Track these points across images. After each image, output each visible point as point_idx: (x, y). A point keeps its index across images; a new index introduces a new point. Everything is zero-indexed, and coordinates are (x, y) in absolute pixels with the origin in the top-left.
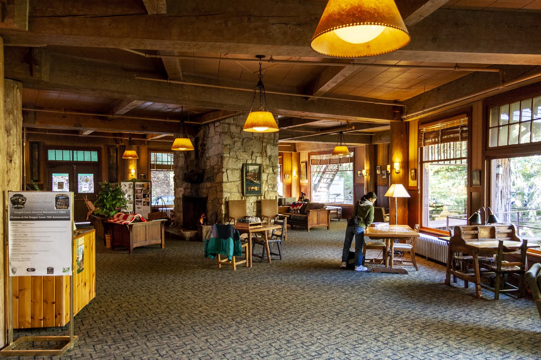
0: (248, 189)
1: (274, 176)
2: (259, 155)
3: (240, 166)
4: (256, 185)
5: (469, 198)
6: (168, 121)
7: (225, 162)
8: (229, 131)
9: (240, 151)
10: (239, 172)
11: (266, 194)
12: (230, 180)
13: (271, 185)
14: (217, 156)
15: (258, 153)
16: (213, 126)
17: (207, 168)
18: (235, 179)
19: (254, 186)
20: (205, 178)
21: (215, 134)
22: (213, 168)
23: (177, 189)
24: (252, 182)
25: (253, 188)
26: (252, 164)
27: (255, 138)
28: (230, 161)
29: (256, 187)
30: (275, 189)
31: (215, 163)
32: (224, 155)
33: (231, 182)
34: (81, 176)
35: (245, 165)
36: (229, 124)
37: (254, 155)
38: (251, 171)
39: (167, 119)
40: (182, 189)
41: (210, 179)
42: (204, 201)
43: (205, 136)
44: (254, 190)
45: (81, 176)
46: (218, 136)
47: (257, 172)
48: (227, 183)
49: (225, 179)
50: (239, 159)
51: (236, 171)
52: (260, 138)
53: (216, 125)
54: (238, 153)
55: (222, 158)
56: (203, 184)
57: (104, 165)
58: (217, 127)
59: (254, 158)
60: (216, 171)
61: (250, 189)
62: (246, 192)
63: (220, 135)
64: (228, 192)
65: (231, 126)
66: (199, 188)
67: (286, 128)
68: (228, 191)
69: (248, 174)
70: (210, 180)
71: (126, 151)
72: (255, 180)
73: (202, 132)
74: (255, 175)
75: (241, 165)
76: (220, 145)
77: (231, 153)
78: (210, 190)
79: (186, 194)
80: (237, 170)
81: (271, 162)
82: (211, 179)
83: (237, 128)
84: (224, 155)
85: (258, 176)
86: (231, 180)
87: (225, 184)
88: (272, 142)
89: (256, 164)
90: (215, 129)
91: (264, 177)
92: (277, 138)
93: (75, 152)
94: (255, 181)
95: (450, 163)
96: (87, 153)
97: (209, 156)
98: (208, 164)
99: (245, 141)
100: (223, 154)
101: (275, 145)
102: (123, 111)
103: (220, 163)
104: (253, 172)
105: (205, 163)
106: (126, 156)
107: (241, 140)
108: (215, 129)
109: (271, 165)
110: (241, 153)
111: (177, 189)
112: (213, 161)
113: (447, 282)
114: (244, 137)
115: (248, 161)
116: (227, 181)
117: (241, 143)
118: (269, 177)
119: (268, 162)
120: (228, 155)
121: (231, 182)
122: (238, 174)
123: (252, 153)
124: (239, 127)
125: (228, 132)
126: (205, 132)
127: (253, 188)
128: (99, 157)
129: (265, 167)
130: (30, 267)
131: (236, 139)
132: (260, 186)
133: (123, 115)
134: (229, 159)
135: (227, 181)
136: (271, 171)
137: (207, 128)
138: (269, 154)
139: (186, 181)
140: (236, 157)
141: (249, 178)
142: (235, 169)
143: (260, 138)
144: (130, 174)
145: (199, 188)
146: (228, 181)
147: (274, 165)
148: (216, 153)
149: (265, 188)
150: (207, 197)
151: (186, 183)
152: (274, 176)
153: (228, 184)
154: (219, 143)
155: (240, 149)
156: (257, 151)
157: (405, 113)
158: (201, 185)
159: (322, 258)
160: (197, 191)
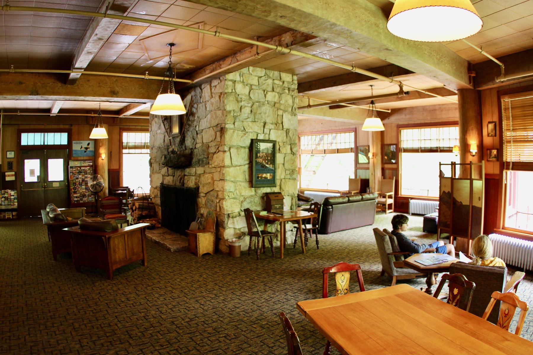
0: (258, 177)
1: (293, 158)
2: (272, 127)
3: (248, 143)
4: (268, 171)
6: (147, 77)
9: (248, 120)
10: (247, 150)
11: (282, 184)
12: (234, 163)
13: (289, 170)
14: (215, 128)
16: (208, 86)
17: (198, 146)
19: (266, 173)
20: (194, 160)
24: (263, 166)
25: (264, 175)
26: (263, 141)
27: (268, 103)
28: (235, 134)
29: (269, 175)
30: (294, 176)
33: (236, 166)
34: (52, 163)
35: (253, 143)
36: (234, 82)
38: (263, 150)
39: (145, 74)
41: (203, 161)
42: (194, 193)
44: (266, 178)
45: (52, 163)
47: (270, 152)
50: (247, 133)
52: (275, 103)
53: (213, 84)
55: (222, 131)
58: (216, 86)
61: (261, 177)
62: (256, 181)
64: (232, 181)
66: (185, 175)
68: (232, 180)
69: (259, 155)
70: (200, 163)
72: (268, 164)
74: (267, 156)
80: (245, 148)
81: (289, 138)
83: (245, 87)
84: (227, 126)
85: (271, 158)
87: (228, 169)
89: (268, 141)
91: (279, 158)
94: (267, 166)
97: (200, 128)
100: (225, 124)
104: (265, 151)
108: (211, 90)
109: (288, 142)
110: (250, 124)
115: (259, 135)
116: (230, 165)
120: (232, 126)
121: (236, 166)
122: (245, 153)
125: (232, 92)
127: (264, 175)
129: (281, 144)
130: (478, 200)
132: (274, 172)
134: (234, 132)
136: (289, 151)
138: (286, 126)
139: (167, 165)
140: (242, 129)
141: (260, 160)
142: (241, 147)
143: (275, 103)
144: (100, 159)
145: (185, 175)
146: (232, 165)
148: (214, 123)
149: (280, 174)
150: (197, 189)
151: (166, 168)
153: (232, 169)
155: (248, 118)
156: (271, 122)
159: (429, 240)
160: (182, 180)
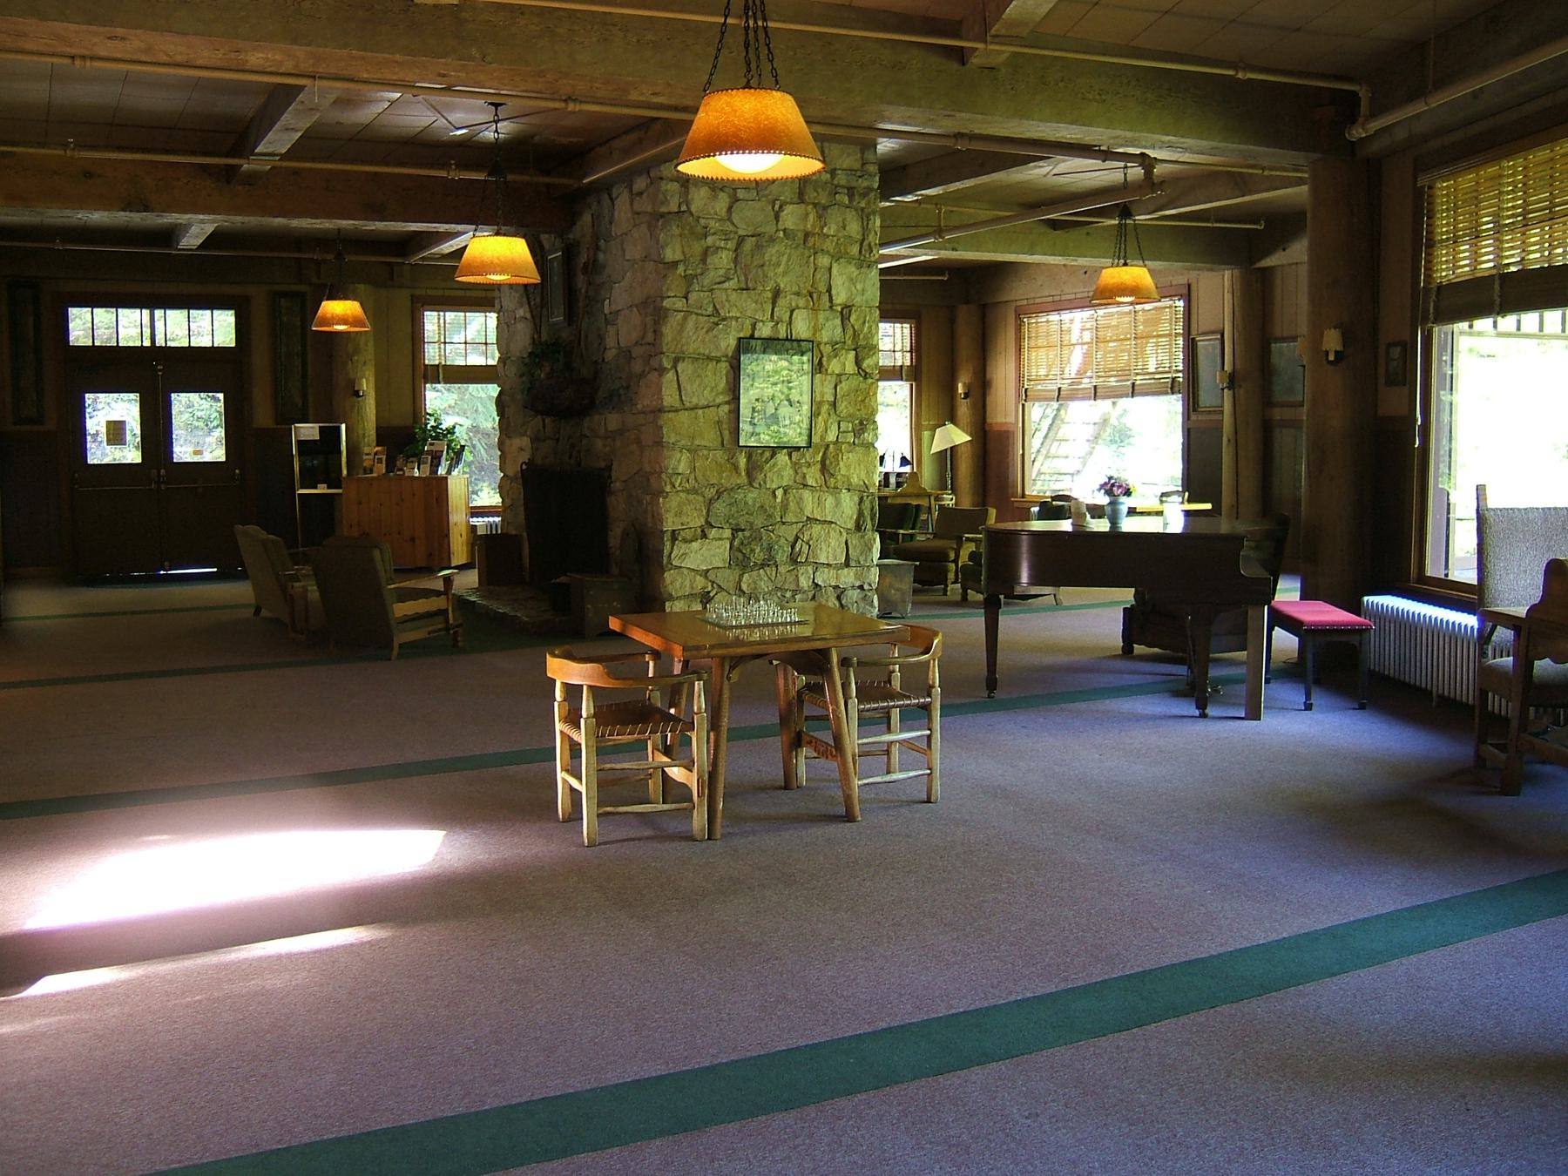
5: (1186, 443)
7: (668, 331)
8: (684, 208)
9: (726, 285)
15: (798, 294)
18: (706, 396)
21: (635, 226)
22: (627, 355)
23: (508, 442)
28: (690, 324)
30: (868, 436)
31: (635, 336)
32: (666, 303)
37: (781, 302)
40: (525, 442)
43: (599, 237)
46: (644, 228)
48: (677, 411)
49: (669, 397)
50: (724, 319)
51: (711, 365)
53: (636, 188)
54: (720, 296)
56: (597, 417)
57: (260, 360)
59: (781, 312)
60: (637, 367)
63: (649, 227)
65: (692, 189)
67: (909, 198)
71: (324, 303)
73: (587, 218)
75: (733, 343)
76: (650, 266)
77: (693, 297)
78: (618, 443)
79: (539, 461)
81: (850, 332)
82: (620, 398)
84: (666, 303)
86: (695, 401)
87: (671, 415)
88: (855, 250)
90: (632, 204)
92: (873, 239)
93: (159, 313)
95: (1471, 327)
96: (202, 317)
97: (614, 308)
98: (610, 342)
99: (749, 244)
100: (663, 298)
101: (863, 263)
102: (277, 141)
103: (650, 337)
105: (601, 338)
106: (327, 321)
107: (731, 245)
108: (632, 204)
110: (733, 296)
111: (508, 442)
112: (623, 332)
113: (1480, 760)
114: (741, 232)
117: (731, 255)
118: (844, 387)
119: (839, 330)
120: (680, 304)
123: (777, 293)
124: (722, 195)
126: (596, 219)
128: (241, 329)
129: (827, 349)
131: (710, 240)
133: (284, 157)
134: (685, 319)
135: (677, 404)
136: (850, 367)
137: (606, 202)
138: (840, 297)
139: (538, 413)
140: (710, 310)
147: (861, 343)
150: (609, 468)
152: (863, 386)
154: (646, 258)
156: (795, 289)
157: (1361, 120)
158: (586, 422)
